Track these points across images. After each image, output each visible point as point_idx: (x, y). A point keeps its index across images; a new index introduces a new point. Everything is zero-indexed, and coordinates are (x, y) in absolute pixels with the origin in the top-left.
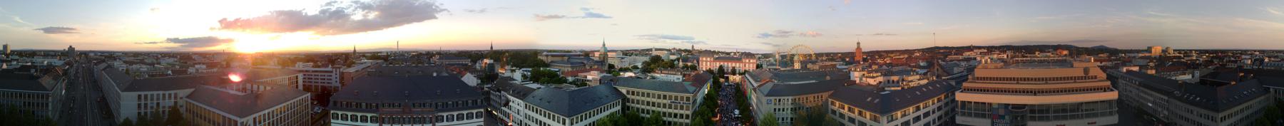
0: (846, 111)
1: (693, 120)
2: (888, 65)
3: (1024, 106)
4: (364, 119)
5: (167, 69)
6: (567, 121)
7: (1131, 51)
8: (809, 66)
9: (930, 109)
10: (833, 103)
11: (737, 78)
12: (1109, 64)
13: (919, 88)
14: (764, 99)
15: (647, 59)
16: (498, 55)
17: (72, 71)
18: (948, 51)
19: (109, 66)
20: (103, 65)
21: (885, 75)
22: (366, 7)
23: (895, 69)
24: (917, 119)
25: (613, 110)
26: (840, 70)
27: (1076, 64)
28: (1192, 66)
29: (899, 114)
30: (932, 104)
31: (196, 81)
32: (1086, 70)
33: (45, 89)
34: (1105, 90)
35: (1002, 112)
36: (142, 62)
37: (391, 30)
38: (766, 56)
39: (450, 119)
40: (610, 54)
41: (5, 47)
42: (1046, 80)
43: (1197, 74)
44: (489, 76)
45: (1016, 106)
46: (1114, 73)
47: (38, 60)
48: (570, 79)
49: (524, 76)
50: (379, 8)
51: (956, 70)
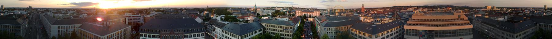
1: (293, 37)
3: (433, 31)
4: (154, 37)
6: (240, 37)
7: (478, 8)
8: (342, 14)
10: (352, 30)
11: (312, 19)
12: (469, 13)
14: (323, 28)
15: (273, 11)
16: (210, 10)
17: (31, 16)
18: (401, 8)
19: (46, 14)
20: (44, 14)
21: (374, 18)
23: (378, 16)
24: (388, 36)
25: (259, 33)
27: (455, 14)
28: (504, 14)
29: (380, 34)
30: (394, 30)
31: (84, 20)
32: (459, 16)
33: (19, 24)
35: (423, 34)
36: (60, 13)
38: (324, 10)
39: (190, 36)
40: (258, 9)
41: (545, 6)
42: (442, 20)
43: (506, 17)
44: (207, 19)
47: (16, 12)
48: (241, 20)
49: (222, 19)
51: (404, 16)
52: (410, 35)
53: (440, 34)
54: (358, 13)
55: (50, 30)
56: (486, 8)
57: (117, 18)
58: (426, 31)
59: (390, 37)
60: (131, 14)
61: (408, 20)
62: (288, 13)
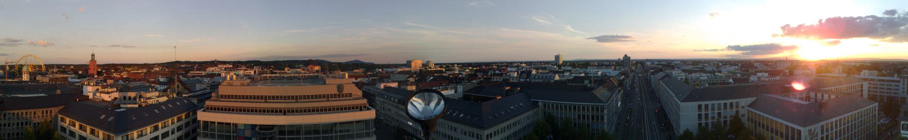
3: (272, 127)
5: (729, 77)
7: (389, 66)
8: (39, 78)
10: (63, 120)
12: (365, 80)
13: (158, 105)
17: (628, 82)
19: (667, 76)
20: (661, 74)
21: (121, 91)
23: (132, 84)
24: (165, 135)
27: (328, 81)
28: (454, 80)
30: (171, 124)
31: (758, 89)
32: (340, 88)
34: (361, 109)
36: (702, 70)
41: (557, 57)
42: (296, 98)
43: (460, 88)
45: (264, 127)
46: (371, 89)
47: (591, 71)
51: (198, 87)
54: (80, 77)
55: (678, 115)
57: (841, 83)
58: (253, 127)
59: (171, 137)
60: (875, 75)
61: (209, 98)
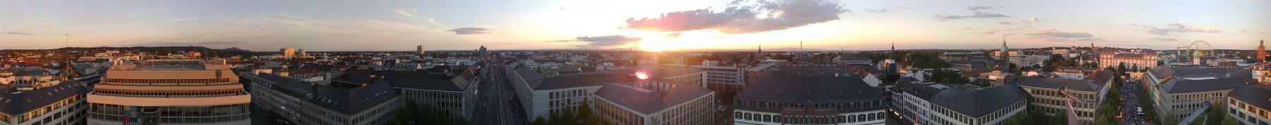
0: (1246, 111)
1: (1097, 118)
2: (21, 65)
3: (155, 109)
4: (767, 119)
6: (975, 122)
7: (264, 53)
8: (1208, 62)
9: (61, 110)
11: (1139, 75)
12: (241, 66)
13: (51, 88)
14: (1169, 96)
15: (1047, 57)
16: (899, 56)
17: (484, 71)
18: (80, 51)
19: (521, 65)
20: (515, 64)
21: (17, 75)
22: (772, 7)
24: (49, 119)
25: (1019, 110)
26: (1241, 68)
27: (207, 66)
28: (324, 68)
29: (30, 114)
30: (63, 105)
31: (605, 78)
32: (218, 73)
34: (237, 93)
35: (134, 115)
37: (795, 29)
38: (1167, 53)
39: (852, 120)
40: (1011, 53)
42: (178, 82)
43: (329, 76)
44: (890, 77)
45: (148, 109)
46: (247, 75)
47: (450, 60)
48: (972, 79)
49: (925, 76)
50: (784, 7)
51: (88, 71)
52: (101, 117)
53: (175, 112)
55: (531, 103)
56: (282, 52)
62: (1081, 62)
